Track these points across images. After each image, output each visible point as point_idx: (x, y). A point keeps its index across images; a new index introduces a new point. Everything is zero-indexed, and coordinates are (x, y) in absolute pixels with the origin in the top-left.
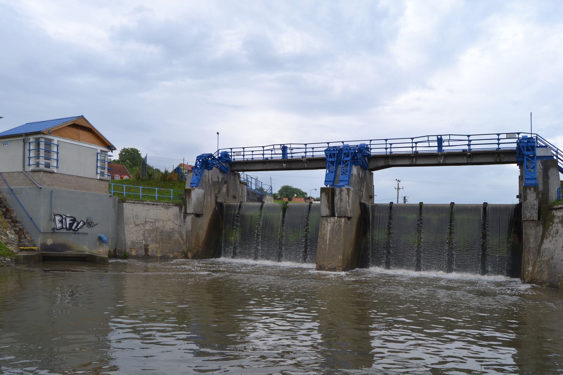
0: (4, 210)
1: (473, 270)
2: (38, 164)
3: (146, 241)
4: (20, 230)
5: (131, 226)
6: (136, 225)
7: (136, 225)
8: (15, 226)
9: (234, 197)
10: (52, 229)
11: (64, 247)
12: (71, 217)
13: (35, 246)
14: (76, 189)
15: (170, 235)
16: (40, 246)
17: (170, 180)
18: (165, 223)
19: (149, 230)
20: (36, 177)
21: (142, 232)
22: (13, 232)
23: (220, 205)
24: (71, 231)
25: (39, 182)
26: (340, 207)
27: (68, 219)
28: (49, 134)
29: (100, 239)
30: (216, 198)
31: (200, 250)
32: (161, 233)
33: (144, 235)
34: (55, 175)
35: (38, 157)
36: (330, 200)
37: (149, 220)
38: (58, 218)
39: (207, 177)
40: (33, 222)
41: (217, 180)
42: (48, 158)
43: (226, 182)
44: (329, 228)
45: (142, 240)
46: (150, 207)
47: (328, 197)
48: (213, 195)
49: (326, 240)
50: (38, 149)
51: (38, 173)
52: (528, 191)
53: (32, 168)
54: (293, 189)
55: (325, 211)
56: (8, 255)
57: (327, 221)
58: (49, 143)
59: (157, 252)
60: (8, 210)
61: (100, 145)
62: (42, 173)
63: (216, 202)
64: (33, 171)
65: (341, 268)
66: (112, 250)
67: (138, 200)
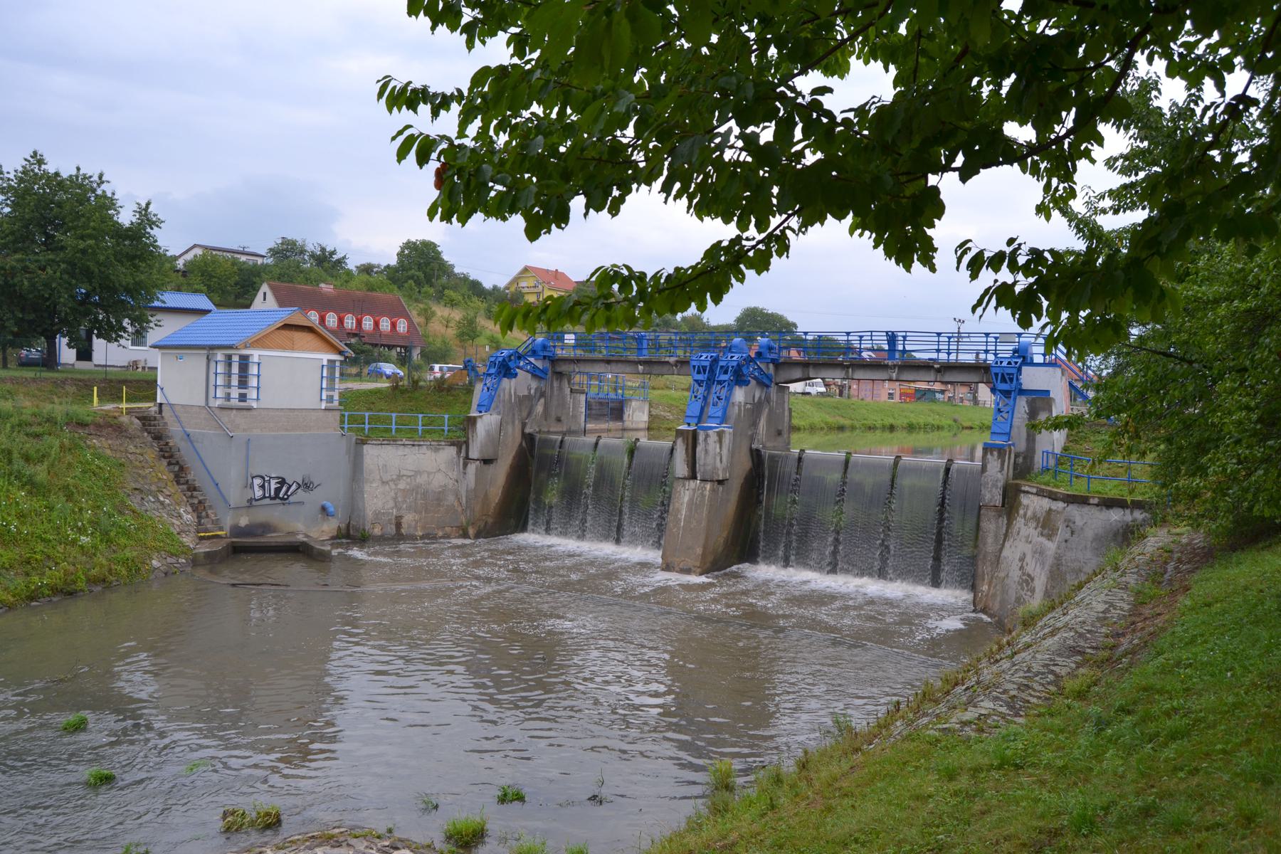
0: (177, 468)
1: (919, 580)
2: (228, 397)
3: (399, 509)
4: (200, 502)
5: (374, 485)
6: (383, 482)
7: (383, 482)
8: (192, 497)
9: (559, 420)
10: (248, 501)
11: (266, 528)
12: (278, 478)
13: (221, 529)
14: (287, 430)
15: (439, 497)
16: (228, 529)
17: (450, 389)
18: (431, 477)
19: (404, 490)
20: (225, 417)
21: (392, 494)
22: (189, 509)
23: (529, 438)
24: (278, 501)
25: (229, 426)
26: (704, 465)
27: (273, 482)
28: (246, 347)
29: (324, 509)
30: (524, 425)
31: (490, 520)
32: (425, 494)
33: (395, 499)
34: (254, 413)
35: (229, 386)
36: (690, 451)
37: (404, 472)
38: (257, 482)
39: (507, 391)
40: (219, 489)
41: (526, 393)
42: (243, 383)
43: (543, 395)
44: (686, 499)
45: (392, 508)
46: (407, 450)
47: (687, 445)
48: (517, 422)
49: (680, 520)
50: (229, 374)
51: (229, 412)
52: (989, 456)
53: (218, 403)
54: (767, 314)
55: (681, 468)
56: (183, 553)
57: (684, 486)
58: (244, 362)
59: (416, 528)
60: (182, 469)
61: (327, 352)
62: (234, 411)
63: (523, 434)
64: (221, 408)
65: (699, 570)
66: (343, 526)
67: (386, 437)
